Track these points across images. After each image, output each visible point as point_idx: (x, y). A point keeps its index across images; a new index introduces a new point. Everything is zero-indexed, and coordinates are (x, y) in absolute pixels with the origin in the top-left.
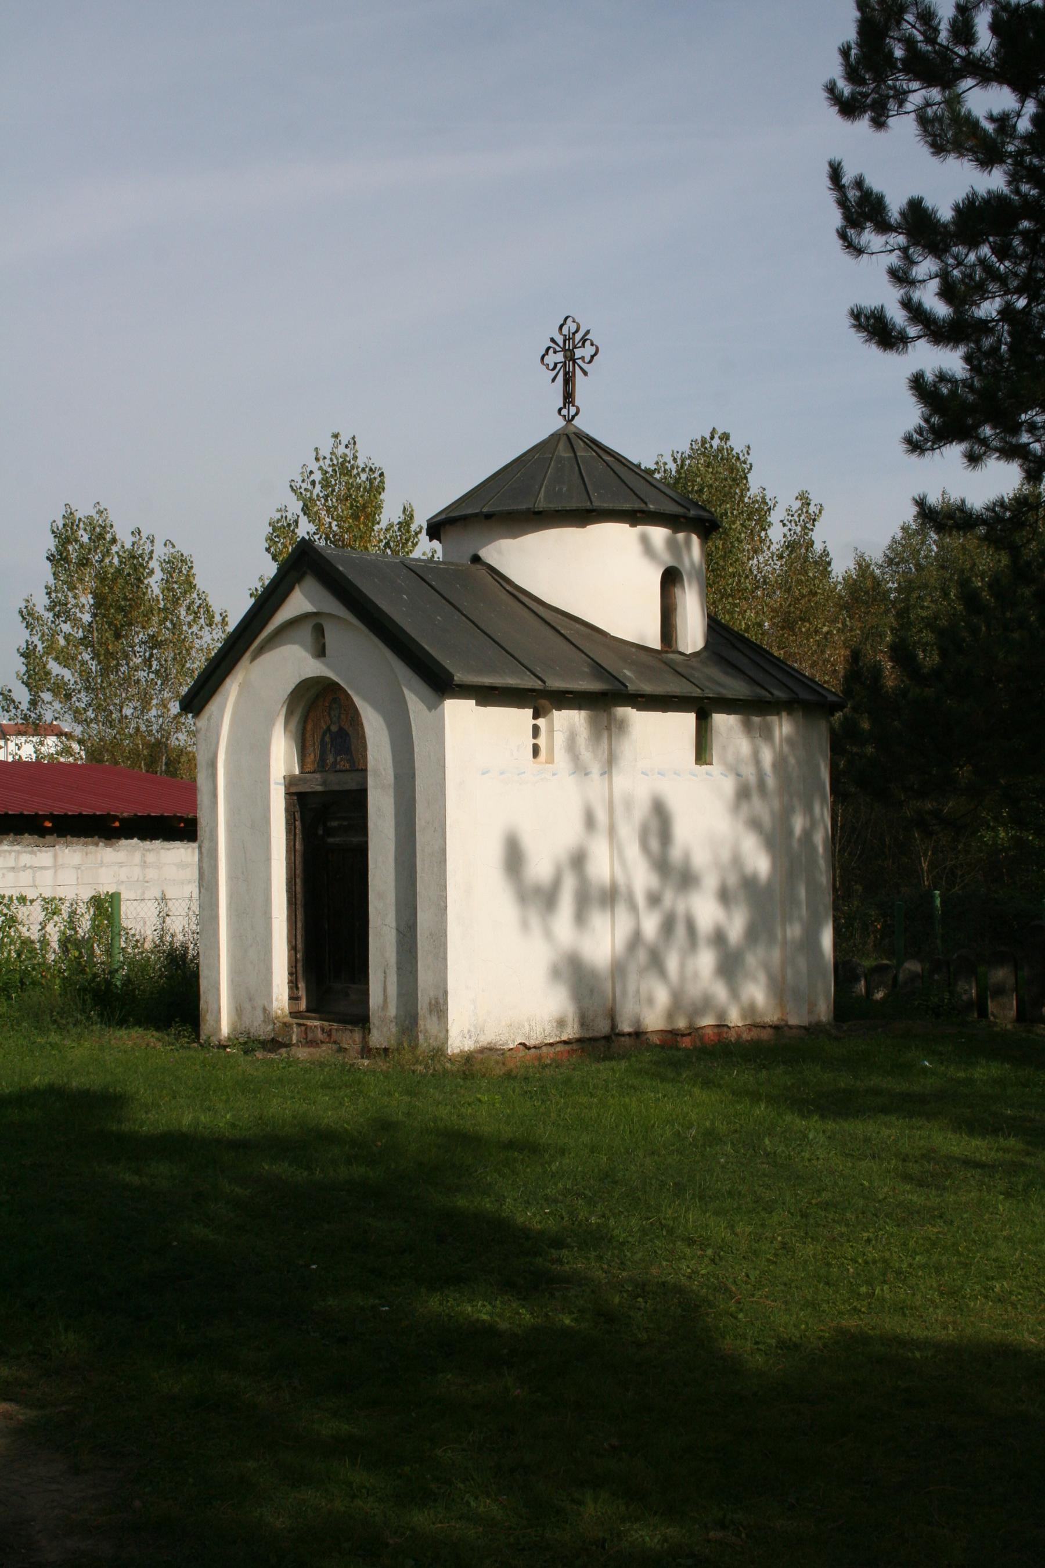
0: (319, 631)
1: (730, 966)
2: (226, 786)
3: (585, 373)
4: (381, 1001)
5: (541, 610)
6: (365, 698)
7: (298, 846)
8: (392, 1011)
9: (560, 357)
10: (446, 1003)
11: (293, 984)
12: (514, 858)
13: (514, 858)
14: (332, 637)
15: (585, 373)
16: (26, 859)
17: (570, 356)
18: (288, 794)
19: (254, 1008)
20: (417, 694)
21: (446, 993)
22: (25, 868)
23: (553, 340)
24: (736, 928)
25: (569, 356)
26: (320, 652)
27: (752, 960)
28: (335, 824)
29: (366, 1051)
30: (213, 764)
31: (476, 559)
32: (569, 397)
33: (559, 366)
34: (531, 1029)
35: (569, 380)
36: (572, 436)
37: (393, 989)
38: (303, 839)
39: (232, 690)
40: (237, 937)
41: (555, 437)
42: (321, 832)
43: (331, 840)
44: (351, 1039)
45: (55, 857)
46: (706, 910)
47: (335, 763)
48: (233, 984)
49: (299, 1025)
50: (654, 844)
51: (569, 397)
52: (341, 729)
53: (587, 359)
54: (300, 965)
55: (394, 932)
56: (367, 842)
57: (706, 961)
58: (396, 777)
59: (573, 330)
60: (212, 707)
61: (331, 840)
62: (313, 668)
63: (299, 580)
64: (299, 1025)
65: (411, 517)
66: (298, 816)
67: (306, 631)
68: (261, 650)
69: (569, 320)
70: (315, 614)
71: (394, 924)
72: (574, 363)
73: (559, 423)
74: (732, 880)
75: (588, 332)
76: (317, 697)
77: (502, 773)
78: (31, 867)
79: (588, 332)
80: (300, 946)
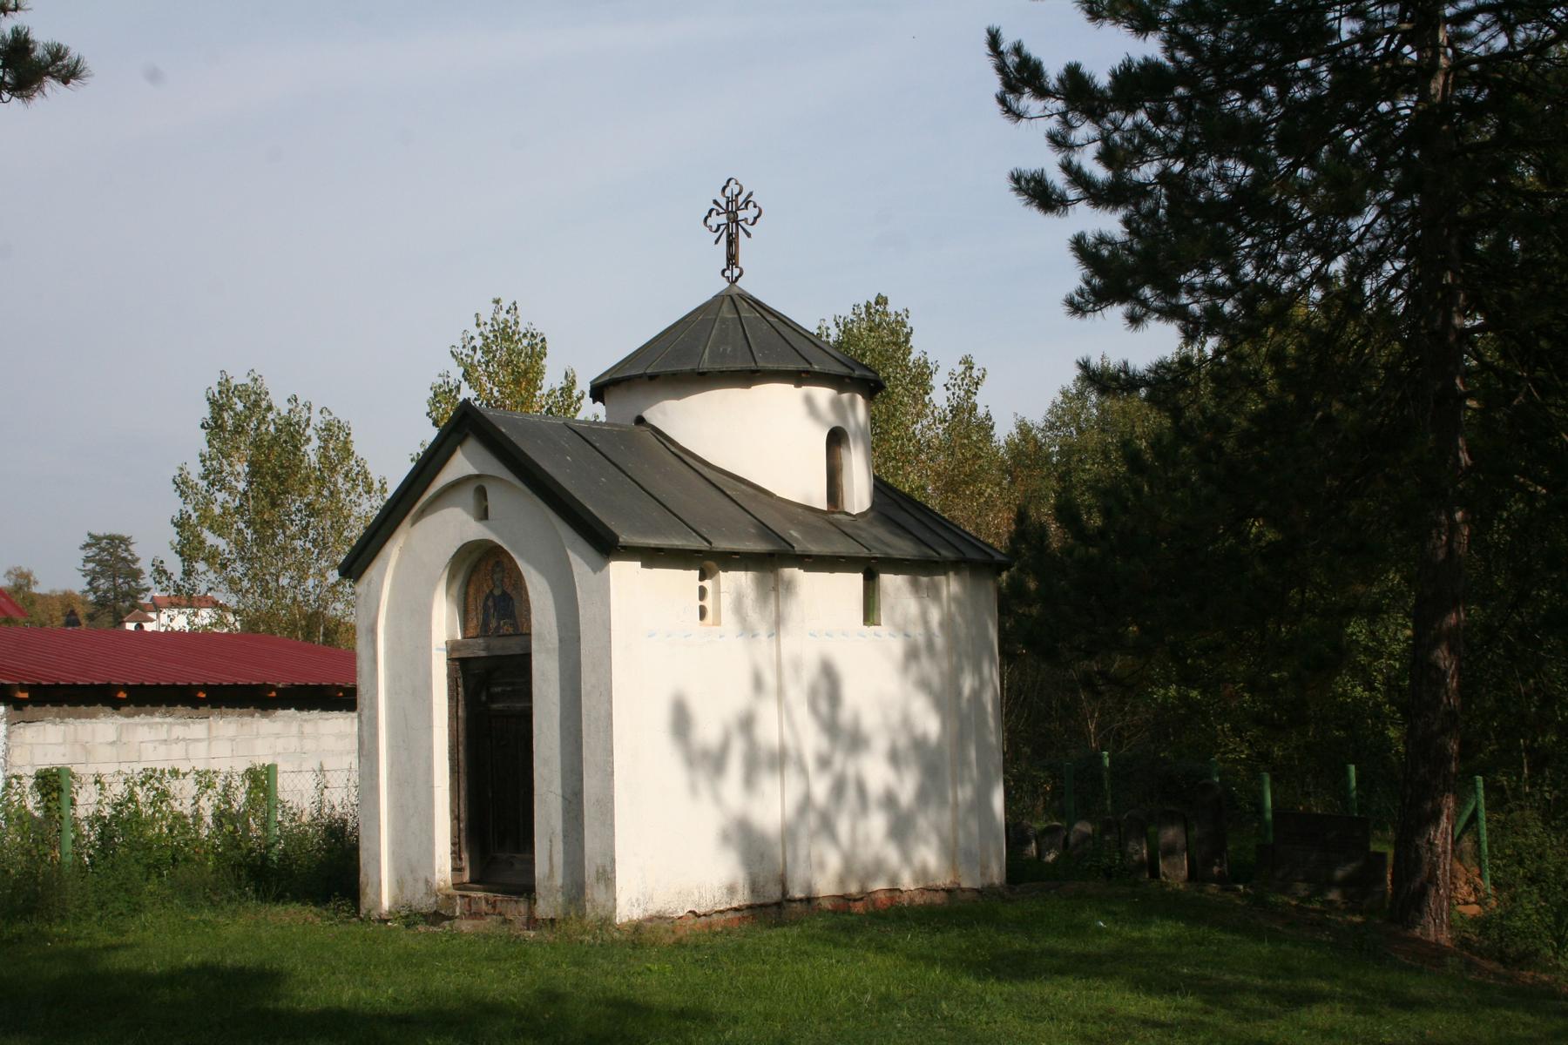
0: (481, 493)
1: (901, 829)
2: (386, 653)
3: (749, 235)
4: (547, 870)
6: (528, 562)
7: (461, 713)
8: (558, 880)
9: (723, 219)
10: (613, 871)
11: (456, 855)
12: (681, 721)
13: (681, 721)
14: (495, 499)
15: (749, 235)
17: (734, 219)
18: (451, 660)
19: (416, 880)
20: (582, 557)
21: (613, 861)
23: (715, 202)
24: (907, 790)
25: (732, 218)
26: (483, 515)
27: (923, 823)
28: (498, 689)
29: (532, 922)
30: (373, 630)
31: (640, 420)
32: (732, 259)
34: (701, 897)
35: (732, 242)
36: (736, 298)
37: (559, 859)
38: (467, 705)
39: (393, 551)
40: (398, 807)
41: (719, 299)
42: (484, 698)
43: (495, 706)
44: (516, 910)
45: (209, 729)
46: (876, 772)
47: (498, 627)
48: (395, 856)
49: (462, 896)
50: (824, 706)
51: (732, 259)
52: (504, 593)
54: (463, 834)
55: (560, 799)
57: (877, 824)
58: (561, 641)
60: (372, 573)
62: (475, 531)
63: (460, 442)
64: (462, 896)
65: (574, 382)
66: (460, 682)
67: (468, 494)
68: (422, 513)
70: (478, 476)
71: (559, 791)
73: (723, 285)
74: (903, 742)
75: (750, 194)
76: (480, 560)
78: (184, 740)
79: (750, 194)
80: (463, 816)
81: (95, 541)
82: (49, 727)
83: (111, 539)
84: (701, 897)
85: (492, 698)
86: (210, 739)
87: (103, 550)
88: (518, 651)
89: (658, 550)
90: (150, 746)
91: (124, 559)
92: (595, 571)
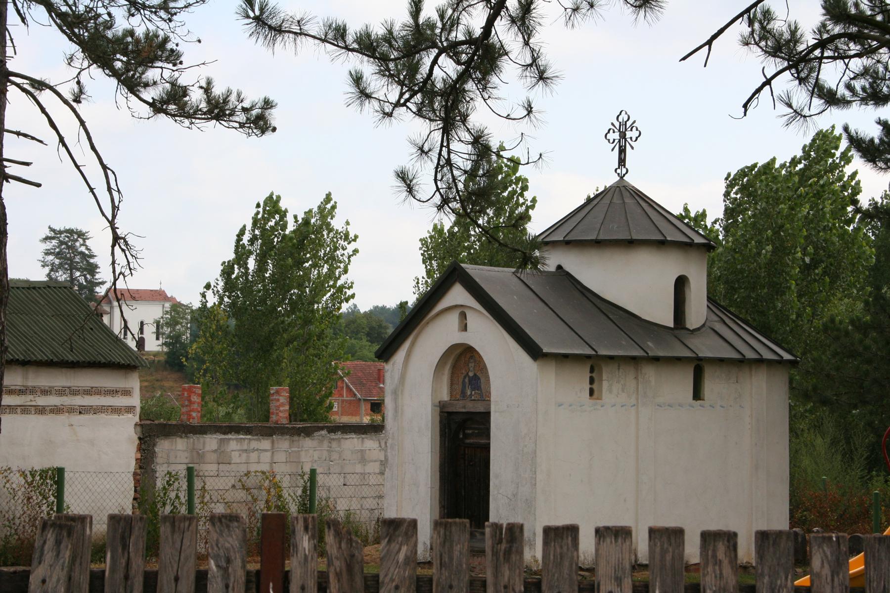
0: (463, 316)
3: (632, 148)
5: (597, 302)
9: (616, 136)
15: (632, 148)
16: (254, 444)
17: (623, 135)
22: (254, 450)
23: (613, 124)
25: (622, 136)
28: (470, 432)
32: (622, 162)
33: (616, 141)
34: (585, 559)
35: (622, 151)
36: (622, 189)
42: (461, 436)
43: (468, 441)
45: (273, 443)
51: (622, 162)
52: (475, 375)
53: (634, 139)
56: (489, 444)
59: (625, 119)
61: (468, 441)
69: (623, 113)
72: (626, 140)
73: (614, 179)
75: (634, 122)
77: (570, 406)
78: (257, 450)
79: (634, 122)
81: (55, 234)
82: (179, 440)
83: (71, 232)
84: (585, 559)
85: (466, 436)
86: (273, 450)
87: (61, 243)
88: (482, 410)
89: (566, 356)
90: (237, 453)
91: (82, 253)
92: (521, 527)
